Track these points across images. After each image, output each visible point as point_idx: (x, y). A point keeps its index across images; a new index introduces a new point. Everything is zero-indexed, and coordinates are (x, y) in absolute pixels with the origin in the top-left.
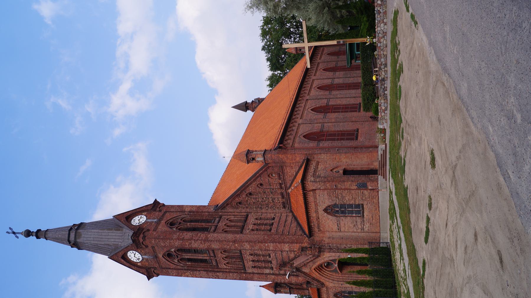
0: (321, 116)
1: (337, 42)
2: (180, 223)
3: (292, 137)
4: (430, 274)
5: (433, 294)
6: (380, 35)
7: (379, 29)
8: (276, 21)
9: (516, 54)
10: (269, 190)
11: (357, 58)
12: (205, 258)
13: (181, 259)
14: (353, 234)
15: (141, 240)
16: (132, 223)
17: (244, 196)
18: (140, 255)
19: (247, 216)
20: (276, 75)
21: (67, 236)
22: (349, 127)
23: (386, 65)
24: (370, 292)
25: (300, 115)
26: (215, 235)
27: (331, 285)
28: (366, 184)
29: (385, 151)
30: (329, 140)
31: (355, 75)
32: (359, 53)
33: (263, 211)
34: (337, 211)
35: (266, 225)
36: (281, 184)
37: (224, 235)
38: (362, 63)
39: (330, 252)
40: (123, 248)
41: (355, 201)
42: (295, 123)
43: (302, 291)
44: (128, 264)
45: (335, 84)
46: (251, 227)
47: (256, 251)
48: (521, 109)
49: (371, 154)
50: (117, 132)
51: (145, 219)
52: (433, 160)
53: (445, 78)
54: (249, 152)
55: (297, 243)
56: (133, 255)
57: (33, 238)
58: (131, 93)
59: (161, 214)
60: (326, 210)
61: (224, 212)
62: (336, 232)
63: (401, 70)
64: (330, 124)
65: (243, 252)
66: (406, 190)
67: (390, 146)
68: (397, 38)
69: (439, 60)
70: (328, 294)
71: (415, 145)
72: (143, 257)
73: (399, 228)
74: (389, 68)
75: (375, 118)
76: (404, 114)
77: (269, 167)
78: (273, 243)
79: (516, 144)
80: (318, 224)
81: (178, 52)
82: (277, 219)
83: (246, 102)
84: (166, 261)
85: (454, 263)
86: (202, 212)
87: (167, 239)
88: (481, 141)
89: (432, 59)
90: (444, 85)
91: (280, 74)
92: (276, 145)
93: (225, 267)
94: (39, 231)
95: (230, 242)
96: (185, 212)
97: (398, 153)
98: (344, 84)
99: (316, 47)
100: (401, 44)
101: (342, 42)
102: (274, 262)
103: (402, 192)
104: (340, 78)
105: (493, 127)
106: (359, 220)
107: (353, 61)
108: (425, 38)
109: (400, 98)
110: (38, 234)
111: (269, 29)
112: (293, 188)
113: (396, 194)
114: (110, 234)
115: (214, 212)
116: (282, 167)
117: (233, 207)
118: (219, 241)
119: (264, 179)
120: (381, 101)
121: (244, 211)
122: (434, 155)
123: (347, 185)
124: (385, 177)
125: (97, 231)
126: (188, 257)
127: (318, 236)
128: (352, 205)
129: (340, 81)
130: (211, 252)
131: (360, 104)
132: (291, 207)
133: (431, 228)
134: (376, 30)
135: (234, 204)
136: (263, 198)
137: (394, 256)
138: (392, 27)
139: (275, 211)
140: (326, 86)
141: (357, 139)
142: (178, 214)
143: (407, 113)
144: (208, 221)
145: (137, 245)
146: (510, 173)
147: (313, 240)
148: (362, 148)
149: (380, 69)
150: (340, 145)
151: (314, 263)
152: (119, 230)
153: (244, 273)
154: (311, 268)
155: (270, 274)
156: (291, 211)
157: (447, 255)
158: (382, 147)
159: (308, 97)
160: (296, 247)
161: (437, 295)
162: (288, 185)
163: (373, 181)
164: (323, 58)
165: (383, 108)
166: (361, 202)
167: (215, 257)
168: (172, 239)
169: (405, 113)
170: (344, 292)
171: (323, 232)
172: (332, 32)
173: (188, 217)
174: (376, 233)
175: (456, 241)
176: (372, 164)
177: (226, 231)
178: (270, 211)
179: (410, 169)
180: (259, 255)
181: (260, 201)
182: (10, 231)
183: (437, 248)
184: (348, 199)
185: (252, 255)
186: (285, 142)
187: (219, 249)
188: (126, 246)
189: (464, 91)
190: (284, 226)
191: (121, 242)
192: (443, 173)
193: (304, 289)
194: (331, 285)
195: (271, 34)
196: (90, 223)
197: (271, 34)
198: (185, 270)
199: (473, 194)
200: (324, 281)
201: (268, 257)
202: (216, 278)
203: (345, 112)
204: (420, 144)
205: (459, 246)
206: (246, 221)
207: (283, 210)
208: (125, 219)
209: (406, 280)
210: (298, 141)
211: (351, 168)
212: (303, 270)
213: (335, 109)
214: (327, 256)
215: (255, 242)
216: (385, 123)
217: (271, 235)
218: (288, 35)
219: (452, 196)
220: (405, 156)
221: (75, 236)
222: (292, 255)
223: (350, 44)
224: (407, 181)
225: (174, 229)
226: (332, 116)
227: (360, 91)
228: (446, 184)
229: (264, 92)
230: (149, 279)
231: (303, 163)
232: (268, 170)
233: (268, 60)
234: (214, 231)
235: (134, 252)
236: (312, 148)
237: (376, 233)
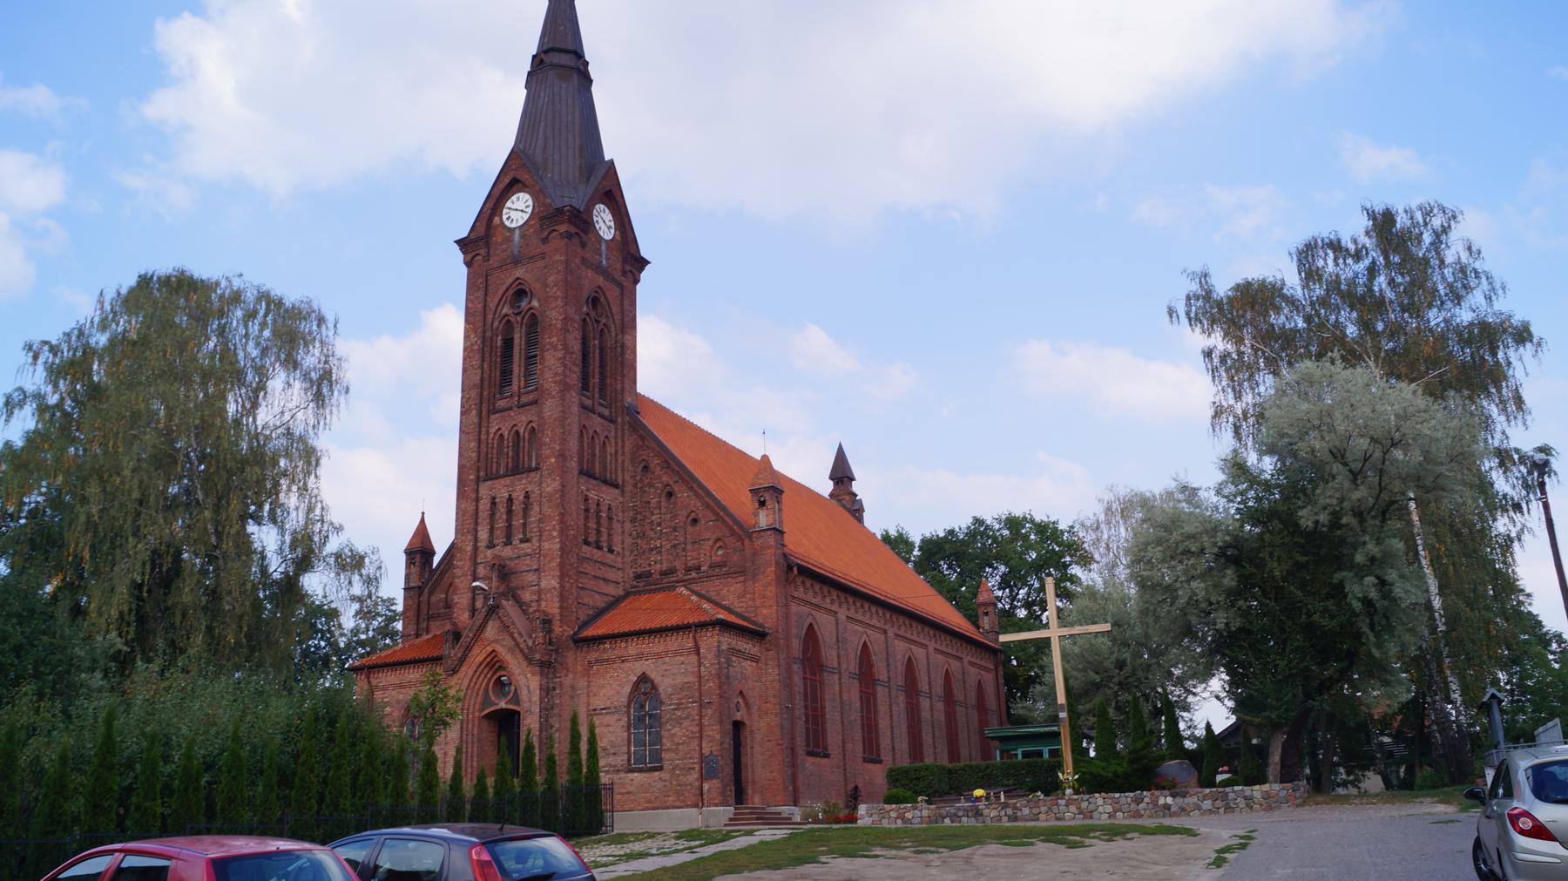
7: (1100, 801)
15: (562, 228)
17: (665, 479)
18: (521, 222)
19: (616, 486)
20: (910, 552)
21: (562, 46)
26: (575, 409)
33: (628, 525)
34: (642, 707)
35: (598, 532)
36: (697, 568)
37: (576, 430)
44: (497, 193)
46: (592, 495)
47: (536, 508)
55: (561, 608)
59: (618, 275)
60: (644, 678)
63: (1073, 845)
64: (837, 688)
65: (533, 474)
78: (561, 549)
82: (610, 558)
83: (852, 479)
98: (919, 721)
102: (507, 552)
107: (997, 743)
111: (1026, 537)
121: (627, 477)
126: (517, 341)
128: (661, 743)
130: (531, 397)
132: (639, 593)
139: (627, 553)
141: (810, 754)
144: (603, 387)
145: (545, 217)
149: (1005, 806)
151: (510, 650)
154: (497, 641)
155: (476, 540)
156: (627, 595)
159: (890, 634)
160: (552, 606)
163: (723, 793)
164: (973, 670)
165: (909, 815)
166: (666, 764)
178: (629, 540)
185: (527, 496)
193: (418, 623)
200: (461, 674)
206: (605, 482)
207: (630, 572)
212: (491, 624)
214: (528, 684)
222: (527, 596)
226: (853, 695)
227: (944, 761)
229: (877, 522)
233: (951, 532)
234: (584, 407)
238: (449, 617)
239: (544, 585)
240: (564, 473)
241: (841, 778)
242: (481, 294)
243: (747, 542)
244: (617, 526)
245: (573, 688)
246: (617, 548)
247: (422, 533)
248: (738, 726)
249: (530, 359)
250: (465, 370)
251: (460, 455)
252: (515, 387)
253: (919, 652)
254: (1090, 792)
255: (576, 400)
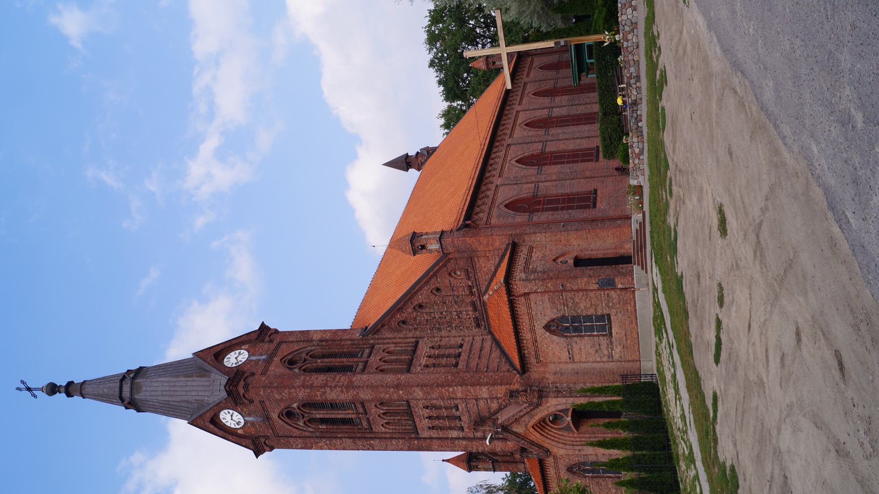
0: (532, 171)
1: (555, 43)
2: (305, 360)
3: (485, 208)
4: (726, 415)
5: (731, 448)
6: (627, 29)
7: (624, 17)
8: (451, 17)
9: (849, 14)
10: (451, 298)
11: (589, 69)
12: (350, 416)
13: (310, 421)
14: (595, 365)
15: (242, 391)
16: (226, 364)
17: (410, 310)
18: (240, 416)
19: (417, 342)
20: (455, 109)
21: (117, 390)
22: (580, 187)
23: (638, 78)
24: (627, 458)
25: (498, 170)
26: (365, 377)
27: (562, 452)
28: (613, 280)
29: (642, 225)
30: (547, 210)
31: (588, 101)
32: (592, 61)
33: (443, 333)
34: (567, 328)
35: (448, 356)
36: (470, 288)
37: (379, 376)
38: (598, 77)
39: (557, 397)
40: (211, 406)
41: (595, 310)
42: (490, 186)
43: (514, 465)
45: (555, 118)
46: (423, 361)
47: (434, 402)
48: (862, 104)
49: (618, 229)
50: (200, 222)
51: (247, 356)
52: (723, 222)
53: (736, 80)
54: (414, 236)
55: (501, 385)
56: (228, 417)
57: (61, 397)
58: (221, 155)
59: (272, 346)
60: (547, 327)
61: (378, 339)
62: (566, 363)
63: (664, 80)
65: (412, 404)
66: (679, 281)
67: (651, 212)
68: (655, 27)
69: (726, 51)
70: (557, 468)
71: (692, 203)
72: (247, 419)
73: (671, 347)
74: (644, 83)
75: (624, 169)
76: (671, 153)
77: (450, 259)
78: (461, 385)
79: (857, 164)
80: (536, 352)
81: (293, 76)
82: (466, 347)
84: (285, 425)
85: (764, 387)
86: (341, 340)
87: (285, 387)
88: (800, 174)
89: (714, 51)
90: (735, 92)
91: (461, 105)
92: (460, 223)
93: (383, 430)
94: (70, 384)
95: (389, 387)
96: (312, 341)
97: (664, 221)
98: (569, 116)
99: (521, 55)
100: (662, 36)
101: (562, 43)
102: (465, 418)
103: (674, 286)
104: (562, 107)
105: (818, 143)
106: (604, 341)
108: (700, 20)
109: (664, 129)
110: (70, 389)
111: (441, 30)
112: (491, 293)
113: (664, 291)
114: (189, 384)
115: (362, 339)
116: (471, 258)
117: (391, 329)
118: (372, 387)
119: (443, 281)
120: (632, 140)
121: (410, 335)
122: (723, 214)
123: (582, 283)
124: (644, 267)
125: (168, 379)
126: (322, 416)
127: (536, 372)
128: (591, 316)
129: (563, 111)
130: (359, 406)
131: (598, 147)
132: (489, 325)
133: (723, 337)
134: (620, 20)
135: (394, 324)
136: (442, 313)
137: (665, 395)
138: (646, 9)
139: (462, 333)
140: (540, 121)
141: (595, 206)
142: (302, 345)
143: (677, 152)
144: (352, 355)
145: (234, 400)
146: (849, 215)
147: (529, 378)
148: (603, 220)
149: (629, 85)
150: (567, 217)
151: (532, 417)
152: (204, 376)
153: (416, 438)
154: (526, 426)
156: (490, 333)
157: (752, 377)
158: (637, 217)
159: (510, 141)
160: (501, 391)
161: (739, 448)
162: (483, 289)
163: (624, 275)
165: (637, 151)
166: (605, 312)
167: (366, 413)
168: (293, 387)
169: (674, 151)
170: (584, 464)
171: (545, 365)
172: (543, 29)
173: (318, 350)
174: (633, 361)
175: (767, 351)
176: (622, 247)
177: (381, 371)
178: (454, 332)
179: (685, 245)
180: (440, 408)
181: (437, 317)
182: (22, 386)
183: (736, 369)
184: (584, 306)
185: (427, 407)
186: (475, 217)
187: (372, 400)
188: (217, 402)
189: (768, 94)
190: (479, 358)
191: (208, 397)
192: (740, 241)
193: (516, 462)
194: (562, 452)
195: (444, 39)
196: (155, 366)
197: (444, 39)
198: (317, 437)
199: (790, 265)
201: (454, 410)
202: (369, 449)
203: (573, 162)
204: (700, 200)
205: (771, 358)
206: (414, 351)
208: (213, 358)
209: (685, 432)
210: (496, 214)
211: (586, 254)
212: (514, 430)
213: (557, 158)
214: (553, 405)
215: (431, 386)
216: (641, 177)
217: (458, 372)
218: (472, 40)
219: (757, 276)
220: (676, 225)
221: (131, 390)
222: (494, 406)
223: (577, 46)
224: (682, 266)
225: (296, 370)
226: (553, 170)
228: (746, 258)
229: (434, 135)
230: (257, 456)
231: (506, 250)
232: (449, 265)
233: (440, 82)
234: (363, 370)
235: (231, 411)
236: (521, 225)
237: (633, 361)
240: (408, 386)
241: (610, 179)
242: (291, 440)
243: (450, 256)
244: (445, 341)
245: (555, 373)
251: (402, 450)
253: (522, 117)
254: (617, 23)
255: (359, 377)
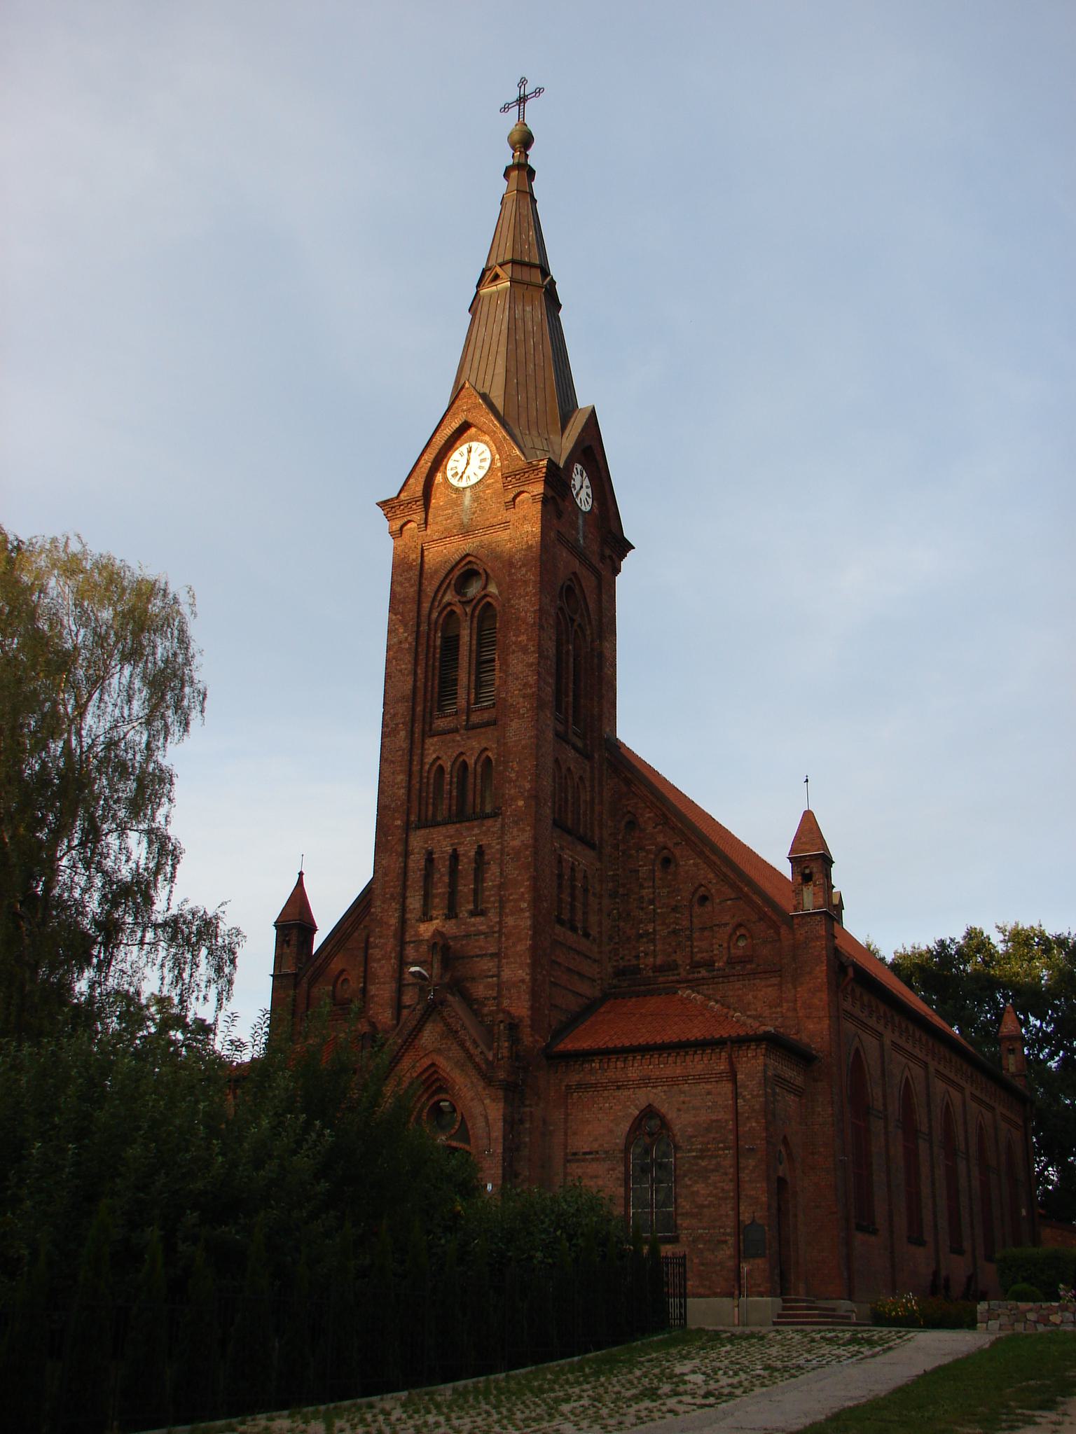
2: (573, 620)
10: (686, 923)
17: (660, 839)
18: (474, 480)
19: (591, 846)
26: (550, 735)
34: (647, 1151)
36: (709, 964)
47: (494, 869)
55: (532, 1008)
57: (507, 157)
59: (595, 561)
60: (649, 1112)
65: (489, 822)
72: (468, 493)
94: (531, 173)
110: (521, 172)
130: (486, 716)
136: (652, 902)
154: (439, 1051)
155: (404, 910)
160: (520, 1007)
165: (1055, 1318)
166: (684, 1234)
167: (470, 727)
181: (644, 892)
185: (480, 851)
190: (569, 970)
201: (471, 907)
222: (480, 990)
238: (363, 1011)
239: (507, 977)
243: (784, 931)
246: (594, 932)
247: (298, 901)
248: (781, 1182)
249: (482, 666)
250: (388, 676)
251: (381, 792)
252: (462, 702)
